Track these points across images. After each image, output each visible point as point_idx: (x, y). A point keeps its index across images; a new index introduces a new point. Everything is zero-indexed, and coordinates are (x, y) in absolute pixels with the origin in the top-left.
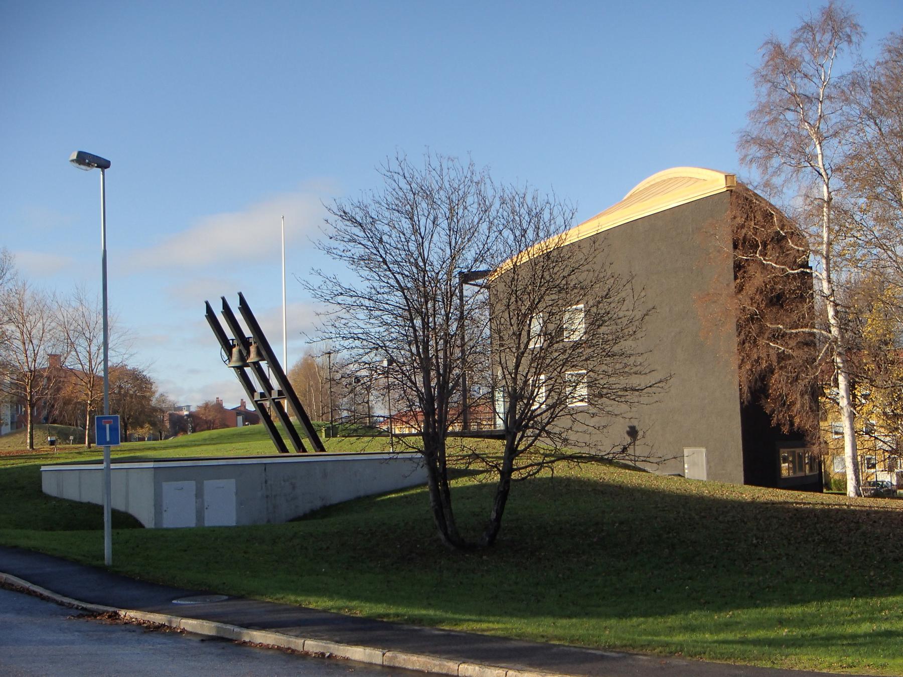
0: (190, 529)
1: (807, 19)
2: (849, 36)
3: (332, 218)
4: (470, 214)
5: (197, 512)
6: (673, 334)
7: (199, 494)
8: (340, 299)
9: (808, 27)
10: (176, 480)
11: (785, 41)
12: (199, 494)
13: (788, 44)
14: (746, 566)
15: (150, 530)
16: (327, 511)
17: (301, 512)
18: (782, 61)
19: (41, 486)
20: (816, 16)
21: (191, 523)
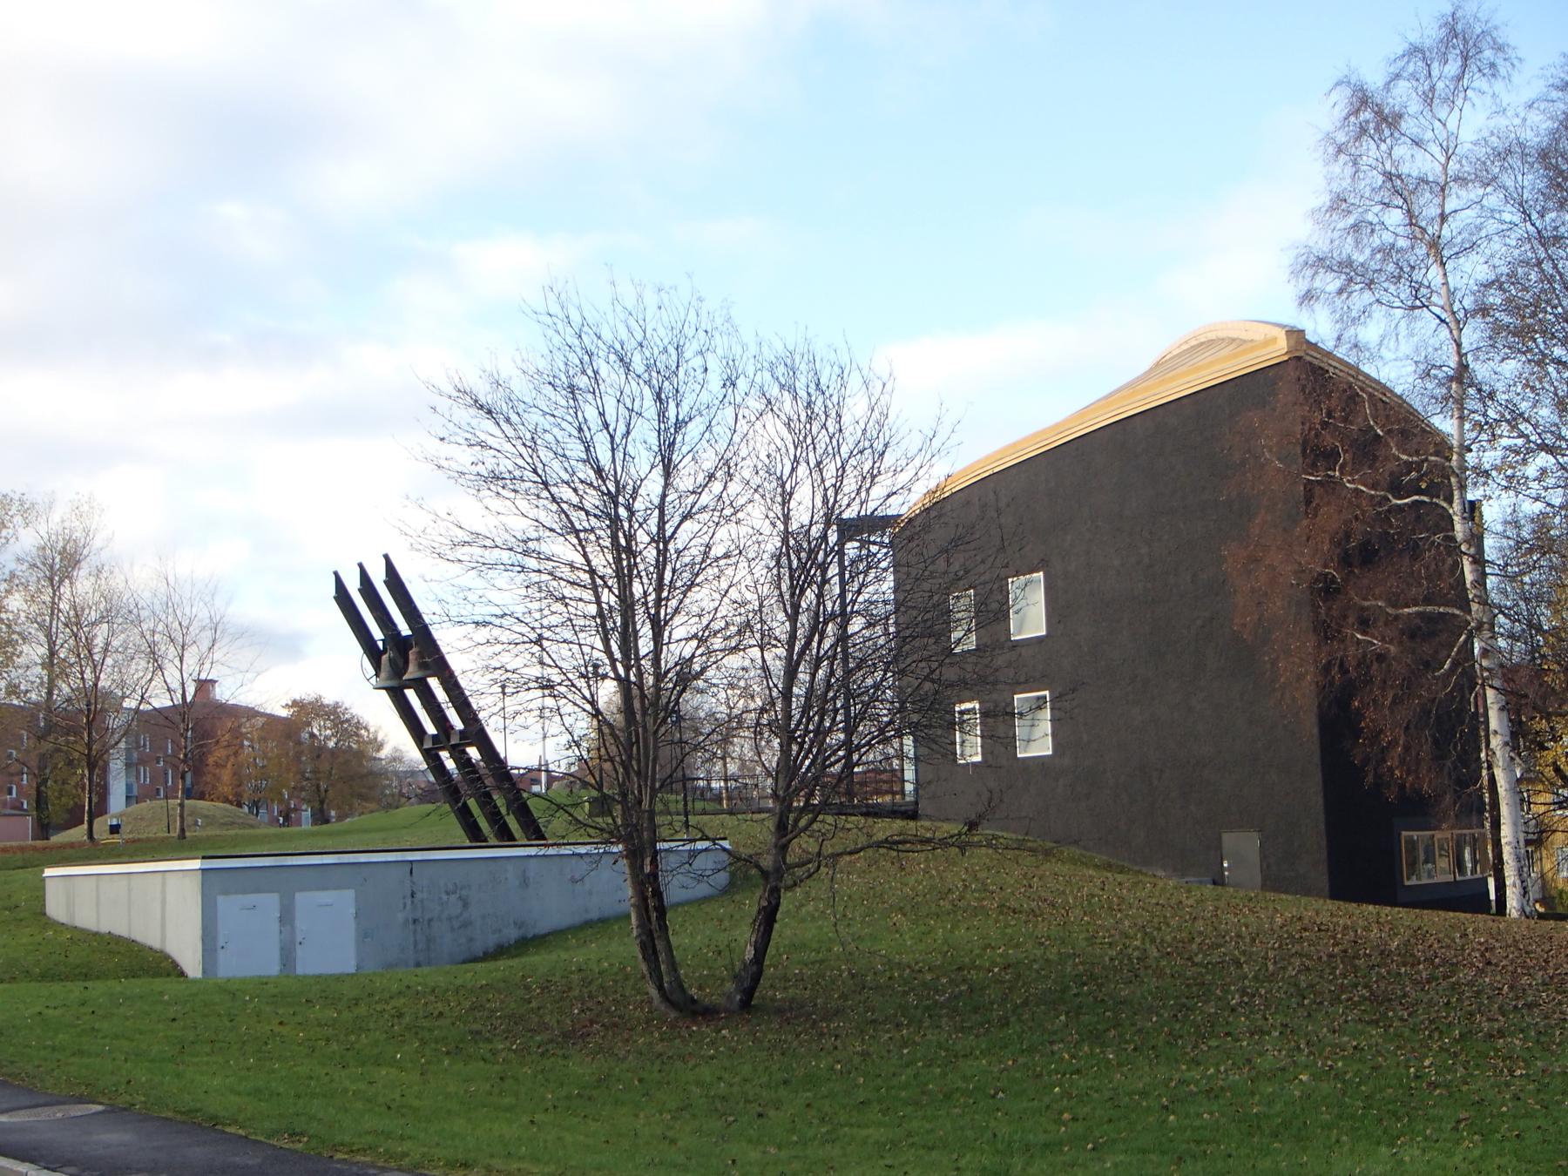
0: (263, 982)
1: (1414, 37)
2: (1492, 65)
3: (443, 404)
4: (699, 392)
5: (282, 949)
6: (1199, 622)
7: (287, 917)
8: (462, 552)
9: (1415, 51)
10: (244, 892)
11: (1374, 79)
12: (287, 917)
13: (1380, 84)
14: (1195, 1047)
15: (195, 981)
16: (525, 944)
17: (478, 948)
18: (1372, 116)
19: (42, 899)
20: (1430, 33)
21: (274, 969)
